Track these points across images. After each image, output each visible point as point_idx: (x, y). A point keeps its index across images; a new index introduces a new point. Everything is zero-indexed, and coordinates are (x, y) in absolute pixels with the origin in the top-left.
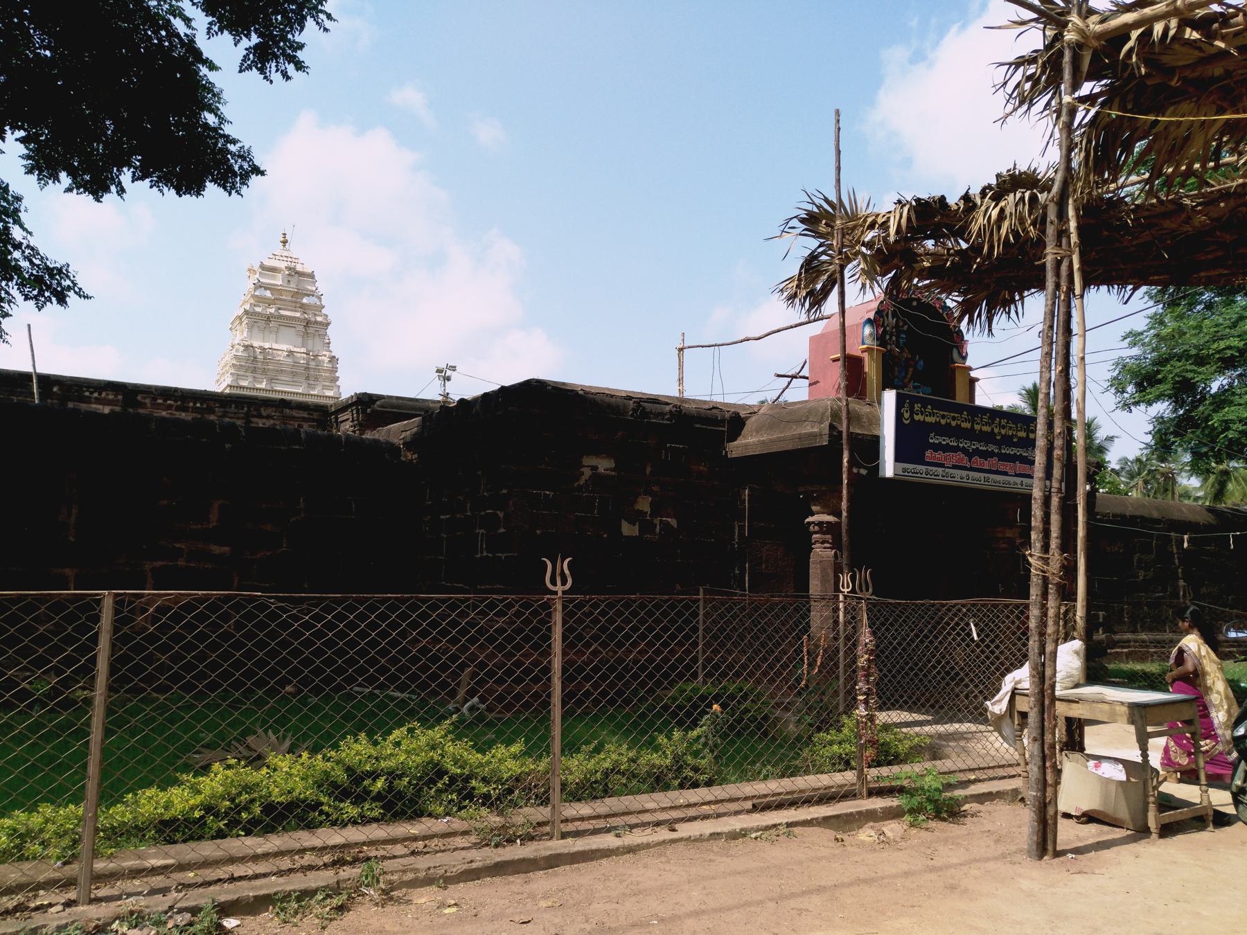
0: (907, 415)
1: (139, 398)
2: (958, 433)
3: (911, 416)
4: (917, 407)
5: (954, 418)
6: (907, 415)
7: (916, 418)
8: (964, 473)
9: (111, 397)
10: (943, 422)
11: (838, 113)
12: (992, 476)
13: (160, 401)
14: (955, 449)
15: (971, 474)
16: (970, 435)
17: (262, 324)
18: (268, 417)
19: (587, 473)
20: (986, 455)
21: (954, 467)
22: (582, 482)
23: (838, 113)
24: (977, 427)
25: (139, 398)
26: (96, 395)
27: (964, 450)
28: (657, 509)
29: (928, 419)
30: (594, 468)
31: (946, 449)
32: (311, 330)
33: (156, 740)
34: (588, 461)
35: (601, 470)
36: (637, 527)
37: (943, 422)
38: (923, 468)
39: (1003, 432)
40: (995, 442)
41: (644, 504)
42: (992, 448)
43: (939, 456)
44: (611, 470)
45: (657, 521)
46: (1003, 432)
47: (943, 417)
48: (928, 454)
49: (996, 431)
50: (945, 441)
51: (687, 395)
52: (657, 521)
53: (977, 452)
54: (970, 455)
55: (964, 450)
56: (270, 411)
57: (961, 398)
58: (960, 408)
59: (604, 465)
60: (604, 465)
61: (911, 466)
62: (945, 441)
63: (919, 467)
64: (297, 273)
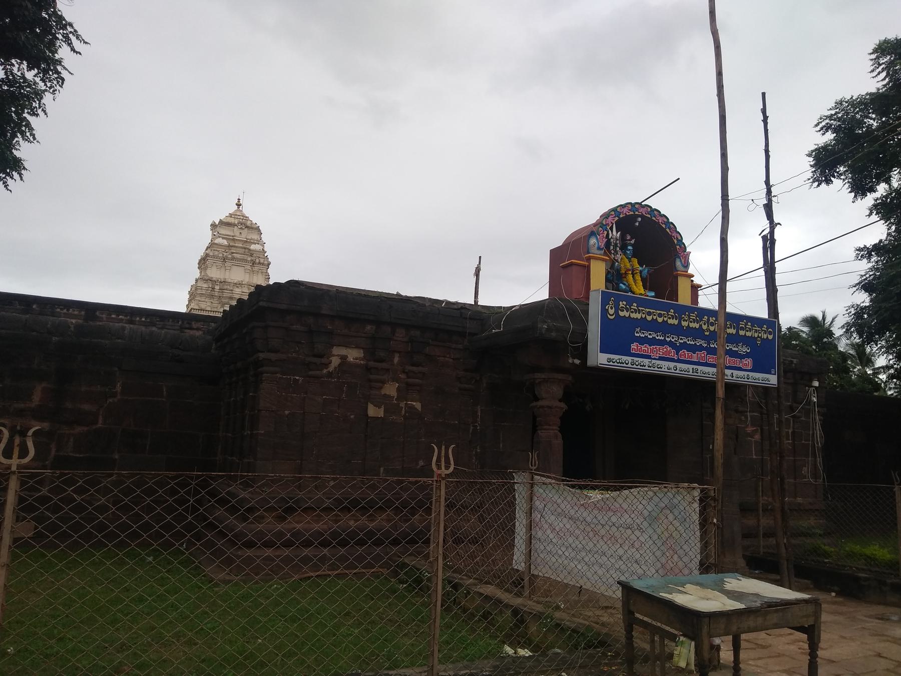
0: (611, 311)
1: (97, 313)
2: (665, 328)
3: (616, 312)
4: (622, 304)
5: (660, 315)
6: (611, 311)
7: (621, 314)
8: (672, 365)
9: (76, 313)
10: (649, 318)
11: (764, 94)
12: (700, 368)
13: (113, 316)
14: (662, 343)
15: (679, 365)
16: (678, 330)
17: (220, 263)
18: (198, 329)
19: (335, 361)
20: (694, 349)
21: (661, 359)
22: (331, 369)
23: (764, 94)
24: (684, 324)
25: (97, 313)
26: (65, 311)
27: (671, 344)
28: (404, 393)
29: (633, 315)
30: (344, 358)
31: (653, 342)
32: (256, 269)
33: (71, 555)
34: (336, 351)
35: (350, 359)
36: (382, 409)
37: (649, 318)
38: (629, 359)
39: (712, 328)
40: (704, 338)
41: (391, 390)
42: (700, 342)
43: (645, 348)
44: (361, 359)
45: (402, 405)
46: (712, 328)
47: (649, 314)
48: (634, 346)
49: (705, 327)
50: (651, 335)
51: (481, 302)
52: (402, 405)
53: (684, 346)
54: (677, 348)
55: (671, 344)
56: (199, 325)
57: (684, 298)
58: (682, 311)
59: (353, 355)
60: (353, 355)
61: (616, 357)
62: (651, 335)
63: (624, 358)
64: (247, 227)
